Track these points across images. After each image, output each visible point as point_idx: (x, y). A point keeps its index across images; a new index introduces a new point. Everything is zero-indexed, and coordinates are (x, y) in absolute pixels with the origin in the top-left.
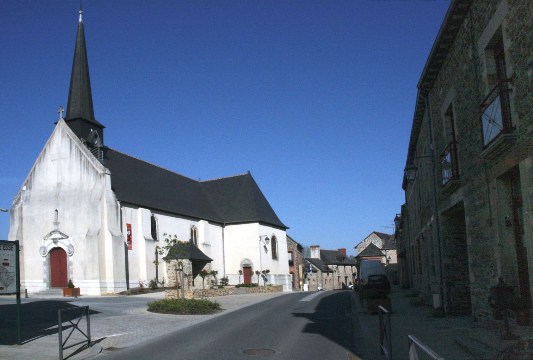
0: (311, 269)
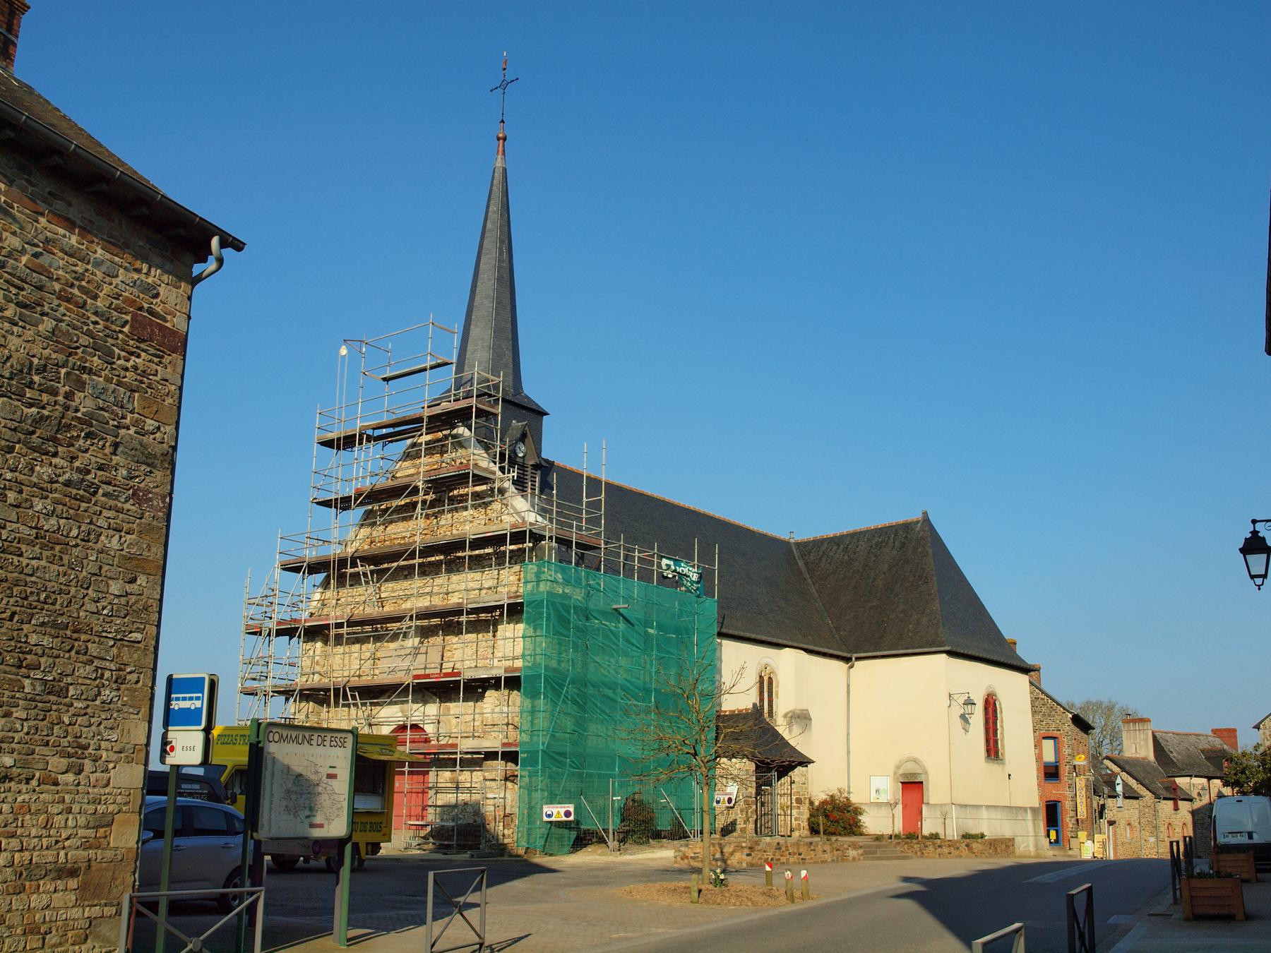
0: (1119, 789)
